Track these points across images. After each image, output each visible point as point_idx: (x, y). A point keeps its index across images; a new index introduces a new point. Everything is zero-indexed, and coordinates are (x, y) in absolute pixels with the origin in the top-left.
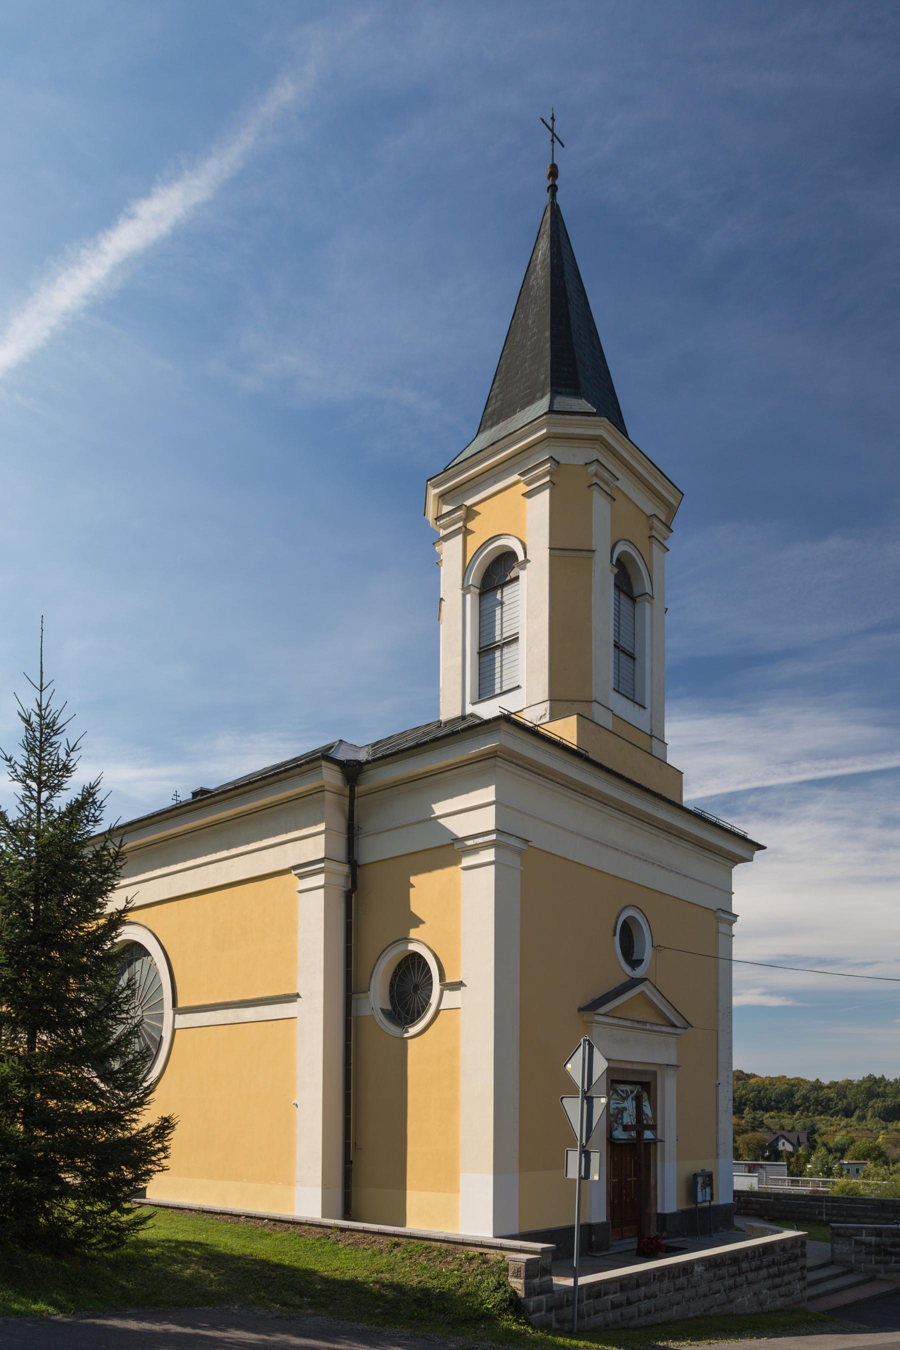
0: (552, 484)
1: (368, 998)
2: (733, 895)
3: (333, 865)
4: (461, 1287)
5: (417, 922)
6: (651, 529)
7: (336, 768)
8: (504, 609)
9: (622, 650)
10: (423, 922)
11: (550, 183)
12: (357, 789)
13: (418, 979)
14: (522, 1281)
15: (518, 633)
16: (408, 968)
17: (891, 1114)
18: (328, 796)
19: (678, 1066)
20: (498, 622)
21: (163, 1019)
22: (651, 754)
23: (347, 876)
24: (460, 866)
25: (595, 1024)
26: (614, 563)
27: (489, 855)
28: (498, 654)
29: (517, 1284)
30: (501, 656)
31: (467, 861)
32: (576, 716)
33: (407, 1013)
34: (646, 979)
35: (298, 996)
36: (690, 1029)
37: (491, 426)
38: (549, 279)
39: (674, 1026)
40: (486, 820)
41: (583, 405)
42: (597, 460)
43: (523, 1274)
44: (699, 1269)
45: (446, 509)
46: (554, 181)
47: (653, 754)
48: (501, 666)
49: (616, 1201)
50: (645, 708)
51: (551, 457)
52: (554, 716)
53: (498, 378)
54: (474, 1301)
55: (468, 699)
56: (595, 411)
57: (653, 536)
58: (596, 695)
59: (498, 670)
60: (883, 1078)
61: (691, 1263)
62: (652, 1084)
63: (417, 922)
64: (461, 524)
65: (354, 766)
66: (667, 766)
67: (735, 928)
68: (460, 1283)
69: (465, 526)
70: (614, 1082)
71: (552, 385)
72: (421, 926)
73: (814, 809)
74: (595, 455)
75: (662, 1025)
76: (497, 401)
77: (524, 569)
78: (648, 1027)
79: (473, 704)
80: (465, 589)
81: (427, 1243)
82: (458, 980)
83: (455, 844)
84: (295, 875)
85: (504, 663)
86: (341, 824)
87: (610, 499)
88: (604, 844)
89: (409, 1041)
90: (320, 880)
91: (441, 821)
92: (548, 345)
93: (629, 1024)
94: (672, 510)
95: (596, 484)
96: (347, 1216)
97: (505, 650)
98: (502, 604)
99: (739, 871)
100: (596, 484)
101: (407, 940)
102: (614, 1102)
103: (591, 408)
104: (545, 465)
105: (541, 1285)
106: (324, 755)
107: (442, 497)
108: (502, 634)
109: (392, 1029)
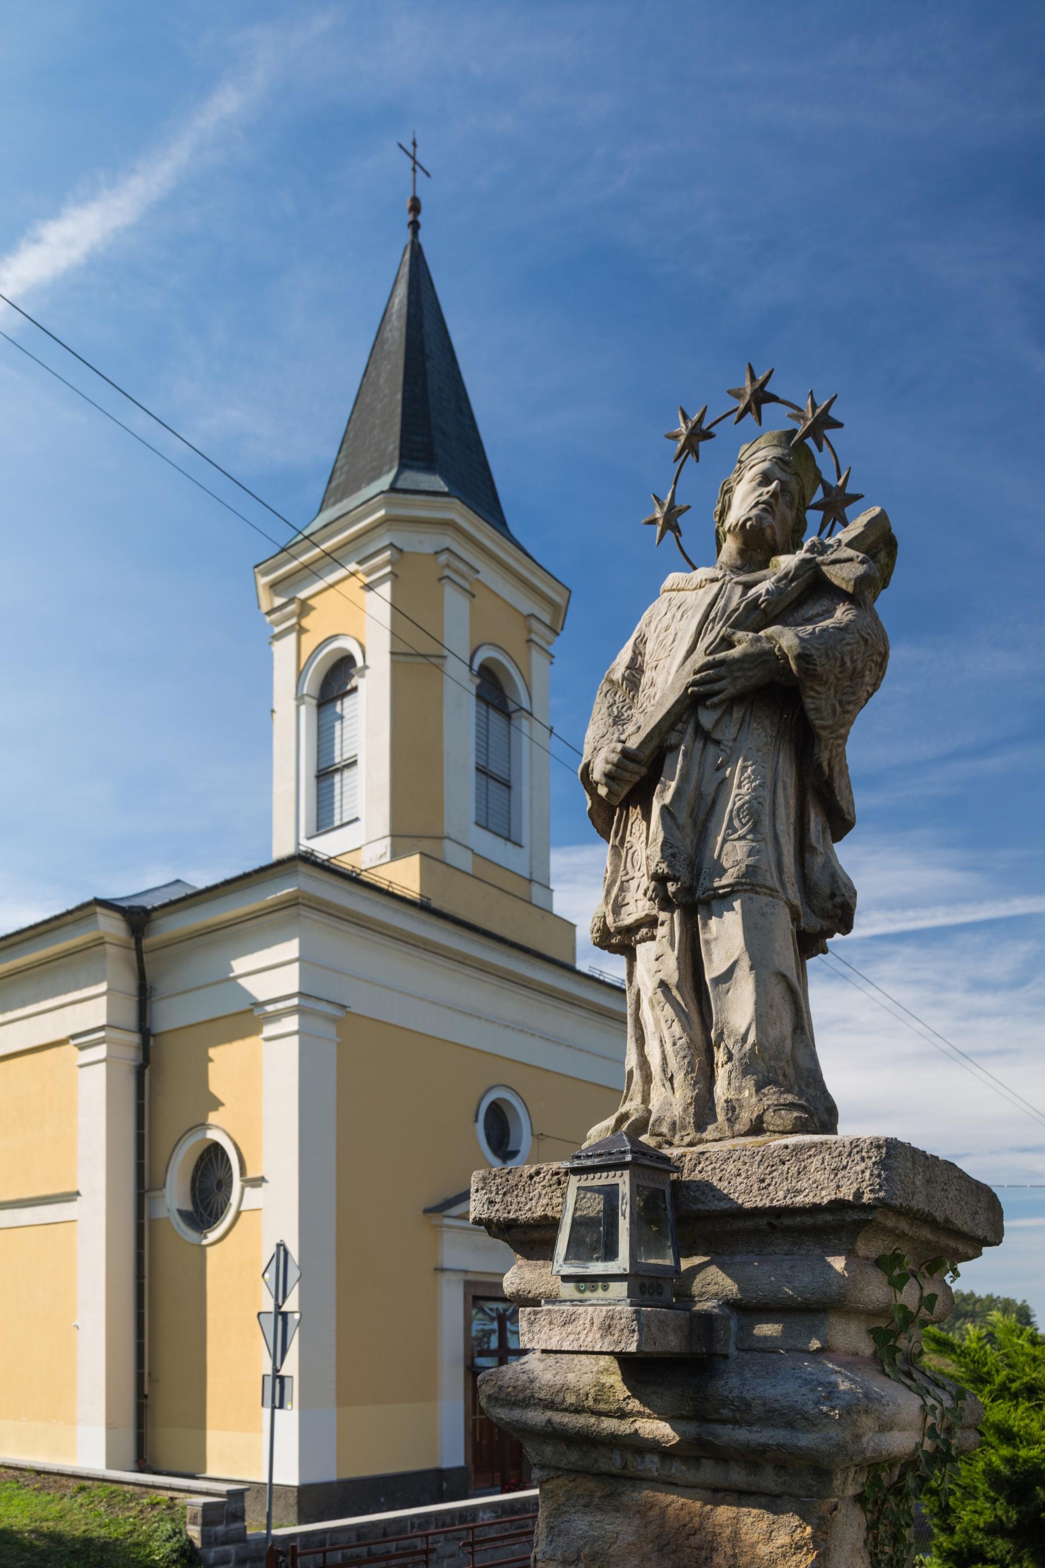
0: (394, 576)
1: (163, 1196)
3: (117, 1035)
4: (131, 1537)
5: (216, 1104)
6: (530, 631)
7: (118, 916)
8: (345, 724)
10: (222, 1104)
12: (146, 942)
13: (220, 1174)
14: (198, 1528)
16: (210, 1160)
18: (110, 950)
20: (337, 740)
22: (530, 902)
23: (137, 1048)
24: (261, 1036)
25: (445, 1229)
26: (476, 666)
27: (292, 1023)
28: (337, 778)
29: (194, 1532)
30: (342, 781)
31: (269, 1030)
33: (210, 1215)
35: (78, 1193)
37: (334, 504)
38: (404, 331)
40: (288, 981)
41: (436, 483)
42: (448, 549)
43: (199, 1520)
44: (485, 1517)
45: (279, 601)
47: (449, 861)
48: (342, 793)
49: (484, 1442)
50: (520, 846)
51: (391, 545)
52: (396, 854)
53: (345, 446)
54: (139, 1553)
56: (446, 489)
58: (449, 829)
59: (337, 798)
60: (972, 1295)
61: (475, 1509)
63: (216, 1104)
64: (294, 621)
65: (138, 913)
68: (131, 1532)
69: (299, 623)
70: (476, 1298)
71: (402, 457)
72: (221, 1109)
73: (888, 969)
76: (341, 474)
77: (362, 676)
79: (309, 838)
80: (300, 699)
81: (115, 1487)
82: (258, 1175)
84: (75, 1045)
85: (345, 789)
86: (130, 984)
88: (460, 1011)
89: (209, 1250)
90: (100, 1052)
91: (241, 981)
92: (399, 410)
94: (559, 612)
95: (447, 577)
96: (142, 1465)
97: (347, 773)
98: (341, 717)
101: (204, 1126)
102: (478, 1322)
104: (384, 553)
105: (226, 1533)
107: (273, 586)
108: (342, 755)
109: (189, 1234)
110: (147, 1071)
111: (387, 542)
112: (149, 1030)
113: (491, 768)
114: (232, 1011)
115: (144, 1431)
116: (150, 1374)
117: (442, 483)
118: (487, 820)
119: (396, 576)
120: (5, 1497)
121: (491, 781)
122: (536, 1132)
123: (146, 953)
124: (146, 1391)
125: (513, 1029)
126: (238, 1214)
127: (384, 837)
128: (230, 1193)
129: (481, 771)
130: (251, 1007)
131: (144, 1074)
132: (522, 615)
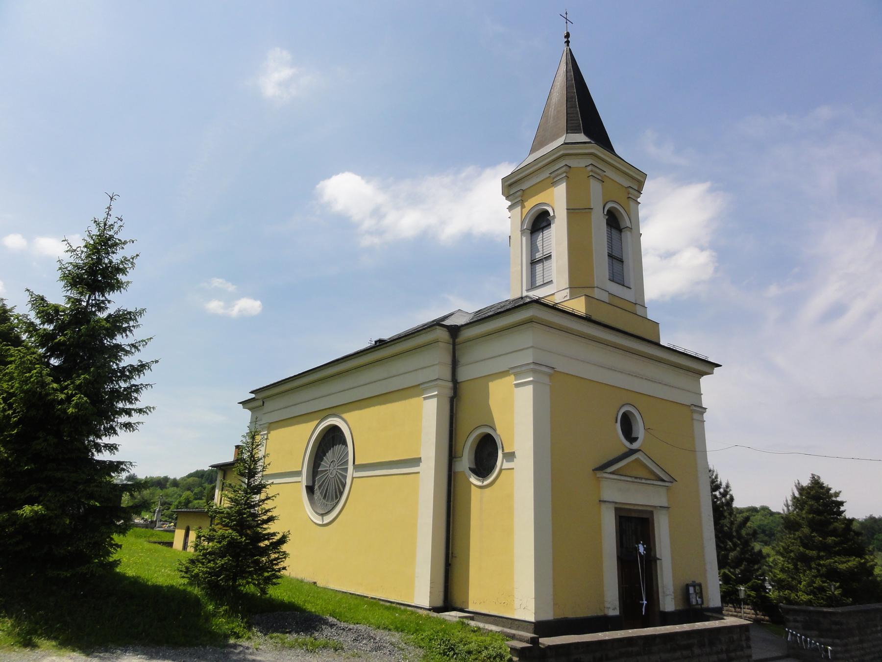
7: (445, 329)
9: (615, 258)
11: (566, 40)
12: (457, 340)
19: (668, 508)
21: (347, 471)
26: (605, 213)
32: (584, 297)
34: (640, 450)
36: (675, 483)
39: (663, 480)
47: (638, 314)
50: (630, 288)
52: (573, 296)
55: (524, 288)
67: (706, 416)
74: (589, 161)
75: (653, 480)
78: (643, 481)
80: (522, 231)
93: (629, 479)
97: (546, 263)
99: (704, 380)
100: (592, 175)
103: (587, 139)
106: (437, 323)
110: (455, 400)
112: (456, 380)
113: (613, 254)
115: (449, 584)
116: (452, 553)
119: (568, 177)
121: (614, 260)
122: (646, 427)
124: (450, 562)
125: (632, 375)
126: (501, 470)
129: (610, 256)
130: (508, 369)
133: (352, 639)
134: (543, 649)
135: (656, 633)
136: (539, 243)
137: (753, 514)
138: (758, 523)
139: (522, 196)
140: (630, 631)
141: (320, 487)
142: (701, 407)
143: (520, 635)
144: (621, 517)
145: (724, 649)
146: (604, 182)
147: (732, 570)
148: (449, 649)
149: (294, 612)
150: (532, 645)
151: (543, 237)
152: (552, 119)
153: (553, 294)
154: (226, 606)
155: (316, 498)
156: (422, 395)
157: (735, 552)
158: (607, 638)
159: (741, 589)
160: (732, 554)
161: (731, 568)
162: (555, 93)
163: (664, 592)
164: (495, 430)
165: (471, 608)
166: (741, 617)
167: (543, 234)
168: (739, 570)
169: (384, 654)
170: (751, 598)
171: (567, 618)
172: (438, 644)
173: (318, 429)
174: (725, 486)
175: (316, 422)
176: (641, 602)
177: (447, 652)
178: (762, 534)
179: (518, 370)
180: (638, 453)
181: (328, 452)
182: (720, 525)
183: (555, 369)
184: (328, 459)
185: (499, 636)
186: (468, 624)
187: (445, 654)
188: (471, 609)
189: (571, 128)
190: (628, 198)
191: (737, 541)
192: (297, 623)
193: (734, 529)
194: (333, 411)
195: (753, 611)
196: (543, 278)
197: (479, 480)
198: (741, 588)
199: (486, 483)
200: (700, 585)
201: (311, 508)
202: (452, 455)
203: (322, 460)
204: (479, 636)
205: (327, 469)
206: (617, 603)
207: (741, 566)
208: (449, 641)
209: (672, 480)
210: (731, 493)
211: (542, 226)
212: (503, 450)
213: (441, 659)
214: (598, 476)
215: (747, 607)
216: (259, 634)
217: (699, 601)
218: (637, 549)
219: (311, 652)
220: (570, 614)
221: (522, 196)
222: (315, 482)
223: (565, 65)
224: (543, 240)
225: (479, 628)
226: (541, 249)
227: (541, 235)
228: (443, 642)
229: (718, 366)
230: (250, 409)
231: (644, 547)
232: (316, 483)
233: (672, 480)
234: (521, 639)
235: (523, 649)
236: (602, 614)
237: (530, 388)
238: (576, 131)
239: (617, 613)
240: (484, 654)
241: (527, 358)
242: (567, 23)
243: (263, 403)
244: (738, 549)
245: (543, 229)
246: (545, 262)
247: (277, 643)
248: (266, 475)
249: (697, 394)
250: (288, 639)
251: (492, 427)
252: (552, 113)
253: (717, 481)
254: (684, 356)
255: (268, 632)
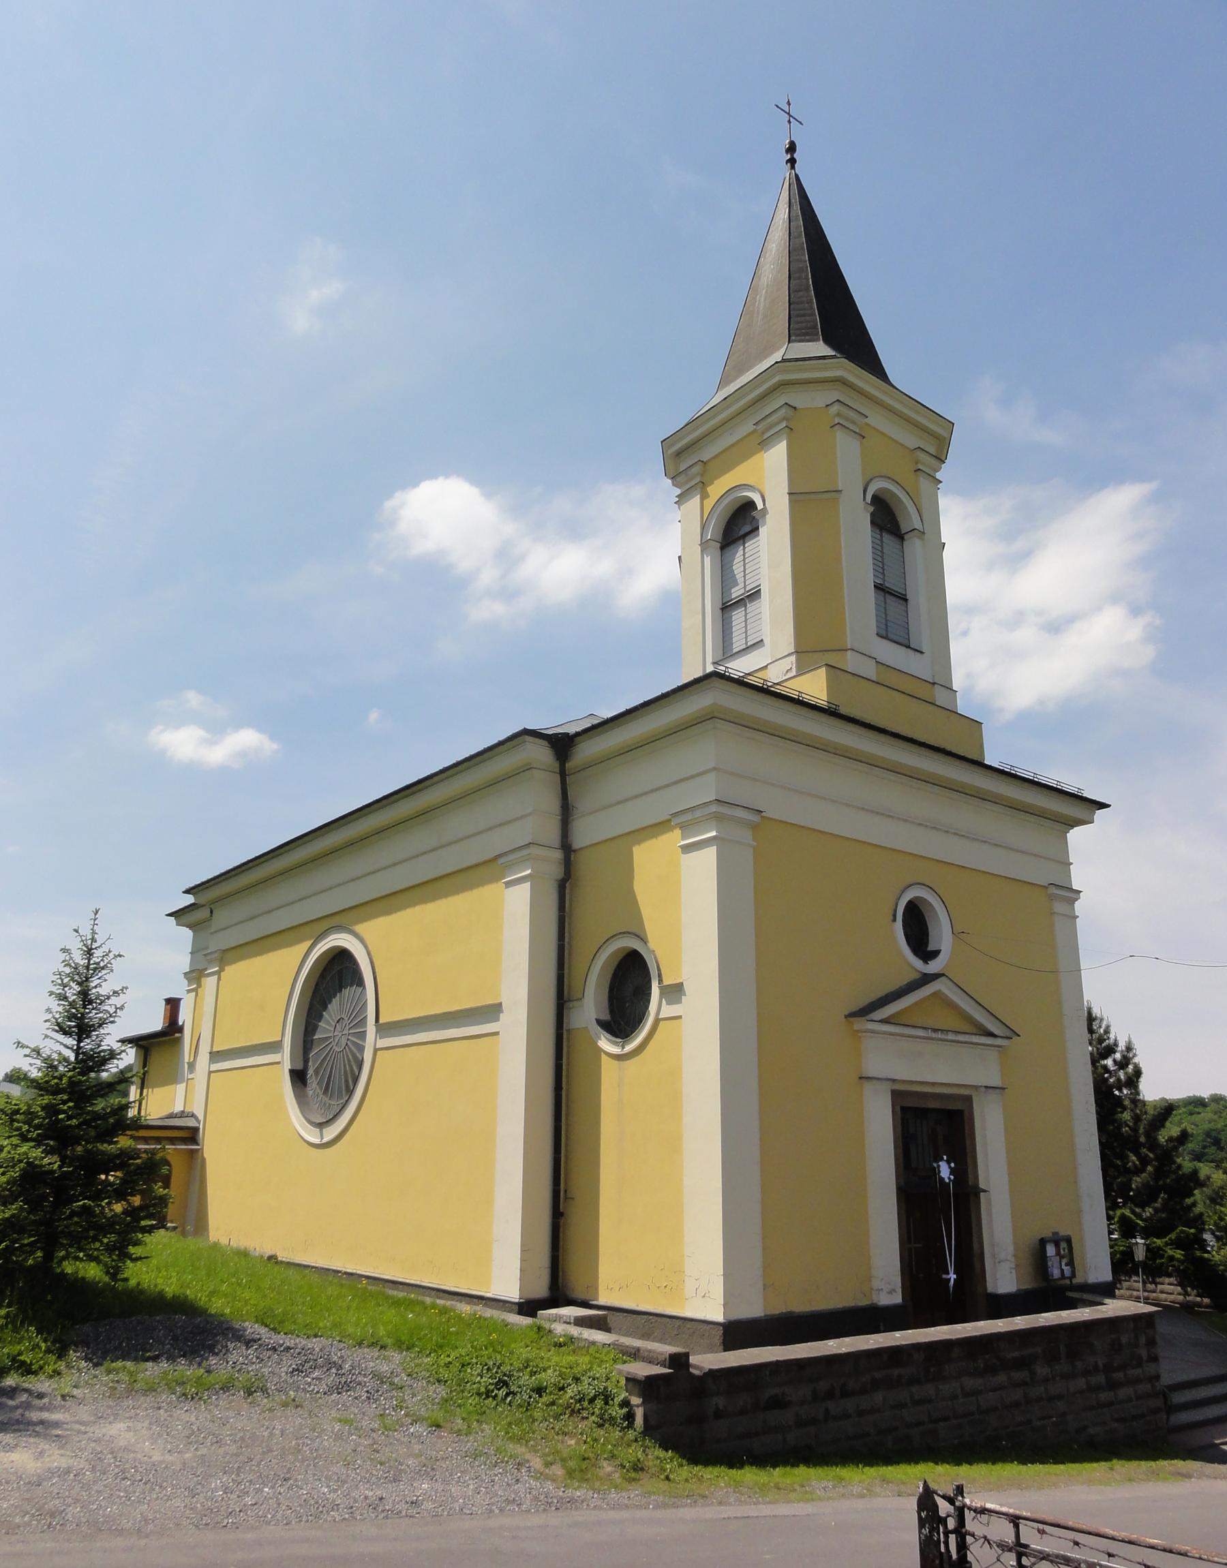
2: (1071, 866)
7: (545, 743)
11: (789, 156)
12: (569, 765)
15: (760, 585)
17: (3, 1423)
34: (943, 975)
36: (1015, 1038)
46: (792, 155)
47: (937, 703)
50: (922, 653)
52: (802, 669)
55: (709, 659)
57: (919, 469)
62: (966, 1113)
66: (958, 716)
74: (835, 395)
75: (972, 1034)
78: (951, 1037)
83: (672, 819)
87: (858, 437)
93: (921, 1033)
97: (751, 607)
99: (1075, 835)
100: (839, 423)
103: (829, 352)
111: (784, 403)
114: (650, 823)
116: (566, 1191)
117: (829, 349)
118: (887, 630)
120: (309, 1378)
121: (887, 595)
122: (958, 929)
123: (568, 775)
125: (926, 826)
126: (657, 1021)
127: (789, 655)
128: (649, 1001)
129: (878, 587)
131: (565, 887)
132: (908, 448)
133: (291, 1369)
134: (699, 1377)
135: (953, 1337)
136: (737, 568)
137: (1197, 1110)
138: (1206, 1127)
139: (702, 475)
140: (898, 1334)
141: (317, 1072)
142: (1071, 890)
143: (650, 1351)
144: (903, 1109)
145: (1100, 1365)
146: (864, 437)
147: (1137, 1210)
148: (497, 1384)
149: (173, 1317)
150: (672, 1371)
151: (744, 555)
152: (760, 317)
153: (766, 667)
154: (9, 1306)
155: (311, 1093)
156: (503, 879)
157: (1144, 1175)
158: (844, 1350)
159: (1137, 1243)
160: (1138, 1179)
161: (1137, 1206)
162: (768, 265)
163: (994, 1256)
164: (644, 940)
165: (605, 1298)
166: (1137, 1299)
167: (744, 549)
168: (1151, 1210)
169: (356, 1398)
170: (1176, 1263)
171: (791, 1312)
172: (478, 1375)
173: (311, 956)
174: (1124, 1048)
175: (308, 944)
176: (944, 1276)
177: (493, 1391)
178: (1213, 1148)
179: (688, 816)
180: (940, 979)
181: (330, 1002)
182: (1116, 1125)
183: (763, 814)
184: (331, 1016)
185: (608, 1352)
186: (550, 1331)
187: (488, 1394)
188: (602, 1300)
189: (797, 332)
190: (915, 471)
191: (1147, 1152)
192: (175, 1338)
193: (1141, 1131)
194: (340, 920)
195: (1179, 1288)
196: (746, 638)
197: (615, 1044)
198: (1139, 1241)
199: (629, 1048)
200: (1069, 1240)
201: (300, 1115)
202: (563, 1001)
203: (320, 1017)
204: (569, 1354)
205: (331, 1035)
206: (897, 1280)
207: (1156, 1201)
208: (499, 1368)
209: (1009, 1033)
210: (1136, 1060)
211: (742, 532)
212: (660, 981)
213: (478, 1407)
214: (856, 1027)
215: (1167, 1280)
216: (83, 1364)
217: (1067, 1270)
218: (935, 1172)
219: (193, 1398)
220: (800, 1305)
221: (702, 475)
222: (308, 1062)
223: (786, 206)
224: (744, 560)
225: (571, 1339)
226: (740, 579)
227: (740, 552)
228: (488, 1369)
229: (1103, 806)
230: (190, 926)
231: (950, 1167)
232: (310, 1064)
233: (1009, 1033)
234: (650, 1359)
235: (650, 1379)
236: (868, 1303)
237: (711, 853)
238: (807, 338)
239: (897, 1299)
240: (570, 1392)
241: (706, 790)
242: (789, 122)
243: (211, 912)
244: (1149, 1168)
245: (744, 537)
246: (748, 605)
247: (118, 1382)
248: (218, 1052)
249: (1062, 863)
250: (148, 1373)
251: (638, 937)
252: (762, 305)
253: (1109, 1038)
254: (1034, 788)
255: (104, 1359)
